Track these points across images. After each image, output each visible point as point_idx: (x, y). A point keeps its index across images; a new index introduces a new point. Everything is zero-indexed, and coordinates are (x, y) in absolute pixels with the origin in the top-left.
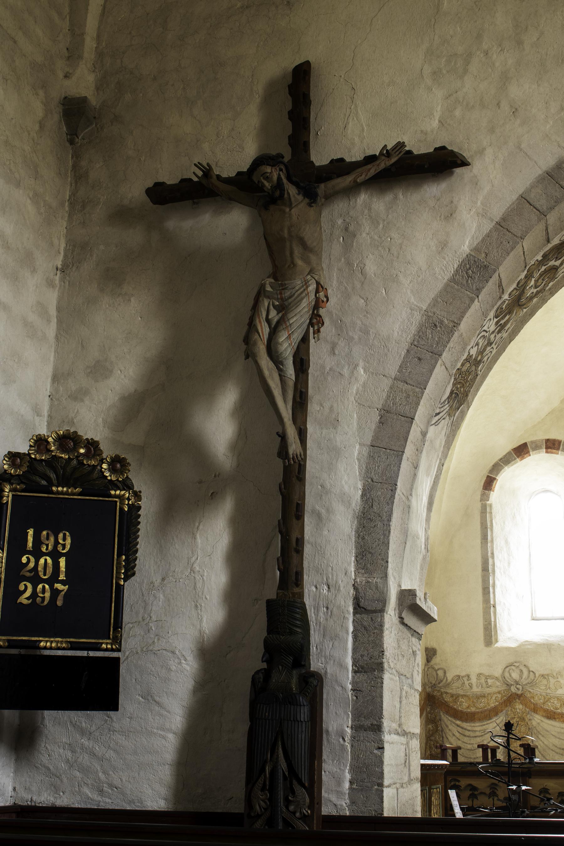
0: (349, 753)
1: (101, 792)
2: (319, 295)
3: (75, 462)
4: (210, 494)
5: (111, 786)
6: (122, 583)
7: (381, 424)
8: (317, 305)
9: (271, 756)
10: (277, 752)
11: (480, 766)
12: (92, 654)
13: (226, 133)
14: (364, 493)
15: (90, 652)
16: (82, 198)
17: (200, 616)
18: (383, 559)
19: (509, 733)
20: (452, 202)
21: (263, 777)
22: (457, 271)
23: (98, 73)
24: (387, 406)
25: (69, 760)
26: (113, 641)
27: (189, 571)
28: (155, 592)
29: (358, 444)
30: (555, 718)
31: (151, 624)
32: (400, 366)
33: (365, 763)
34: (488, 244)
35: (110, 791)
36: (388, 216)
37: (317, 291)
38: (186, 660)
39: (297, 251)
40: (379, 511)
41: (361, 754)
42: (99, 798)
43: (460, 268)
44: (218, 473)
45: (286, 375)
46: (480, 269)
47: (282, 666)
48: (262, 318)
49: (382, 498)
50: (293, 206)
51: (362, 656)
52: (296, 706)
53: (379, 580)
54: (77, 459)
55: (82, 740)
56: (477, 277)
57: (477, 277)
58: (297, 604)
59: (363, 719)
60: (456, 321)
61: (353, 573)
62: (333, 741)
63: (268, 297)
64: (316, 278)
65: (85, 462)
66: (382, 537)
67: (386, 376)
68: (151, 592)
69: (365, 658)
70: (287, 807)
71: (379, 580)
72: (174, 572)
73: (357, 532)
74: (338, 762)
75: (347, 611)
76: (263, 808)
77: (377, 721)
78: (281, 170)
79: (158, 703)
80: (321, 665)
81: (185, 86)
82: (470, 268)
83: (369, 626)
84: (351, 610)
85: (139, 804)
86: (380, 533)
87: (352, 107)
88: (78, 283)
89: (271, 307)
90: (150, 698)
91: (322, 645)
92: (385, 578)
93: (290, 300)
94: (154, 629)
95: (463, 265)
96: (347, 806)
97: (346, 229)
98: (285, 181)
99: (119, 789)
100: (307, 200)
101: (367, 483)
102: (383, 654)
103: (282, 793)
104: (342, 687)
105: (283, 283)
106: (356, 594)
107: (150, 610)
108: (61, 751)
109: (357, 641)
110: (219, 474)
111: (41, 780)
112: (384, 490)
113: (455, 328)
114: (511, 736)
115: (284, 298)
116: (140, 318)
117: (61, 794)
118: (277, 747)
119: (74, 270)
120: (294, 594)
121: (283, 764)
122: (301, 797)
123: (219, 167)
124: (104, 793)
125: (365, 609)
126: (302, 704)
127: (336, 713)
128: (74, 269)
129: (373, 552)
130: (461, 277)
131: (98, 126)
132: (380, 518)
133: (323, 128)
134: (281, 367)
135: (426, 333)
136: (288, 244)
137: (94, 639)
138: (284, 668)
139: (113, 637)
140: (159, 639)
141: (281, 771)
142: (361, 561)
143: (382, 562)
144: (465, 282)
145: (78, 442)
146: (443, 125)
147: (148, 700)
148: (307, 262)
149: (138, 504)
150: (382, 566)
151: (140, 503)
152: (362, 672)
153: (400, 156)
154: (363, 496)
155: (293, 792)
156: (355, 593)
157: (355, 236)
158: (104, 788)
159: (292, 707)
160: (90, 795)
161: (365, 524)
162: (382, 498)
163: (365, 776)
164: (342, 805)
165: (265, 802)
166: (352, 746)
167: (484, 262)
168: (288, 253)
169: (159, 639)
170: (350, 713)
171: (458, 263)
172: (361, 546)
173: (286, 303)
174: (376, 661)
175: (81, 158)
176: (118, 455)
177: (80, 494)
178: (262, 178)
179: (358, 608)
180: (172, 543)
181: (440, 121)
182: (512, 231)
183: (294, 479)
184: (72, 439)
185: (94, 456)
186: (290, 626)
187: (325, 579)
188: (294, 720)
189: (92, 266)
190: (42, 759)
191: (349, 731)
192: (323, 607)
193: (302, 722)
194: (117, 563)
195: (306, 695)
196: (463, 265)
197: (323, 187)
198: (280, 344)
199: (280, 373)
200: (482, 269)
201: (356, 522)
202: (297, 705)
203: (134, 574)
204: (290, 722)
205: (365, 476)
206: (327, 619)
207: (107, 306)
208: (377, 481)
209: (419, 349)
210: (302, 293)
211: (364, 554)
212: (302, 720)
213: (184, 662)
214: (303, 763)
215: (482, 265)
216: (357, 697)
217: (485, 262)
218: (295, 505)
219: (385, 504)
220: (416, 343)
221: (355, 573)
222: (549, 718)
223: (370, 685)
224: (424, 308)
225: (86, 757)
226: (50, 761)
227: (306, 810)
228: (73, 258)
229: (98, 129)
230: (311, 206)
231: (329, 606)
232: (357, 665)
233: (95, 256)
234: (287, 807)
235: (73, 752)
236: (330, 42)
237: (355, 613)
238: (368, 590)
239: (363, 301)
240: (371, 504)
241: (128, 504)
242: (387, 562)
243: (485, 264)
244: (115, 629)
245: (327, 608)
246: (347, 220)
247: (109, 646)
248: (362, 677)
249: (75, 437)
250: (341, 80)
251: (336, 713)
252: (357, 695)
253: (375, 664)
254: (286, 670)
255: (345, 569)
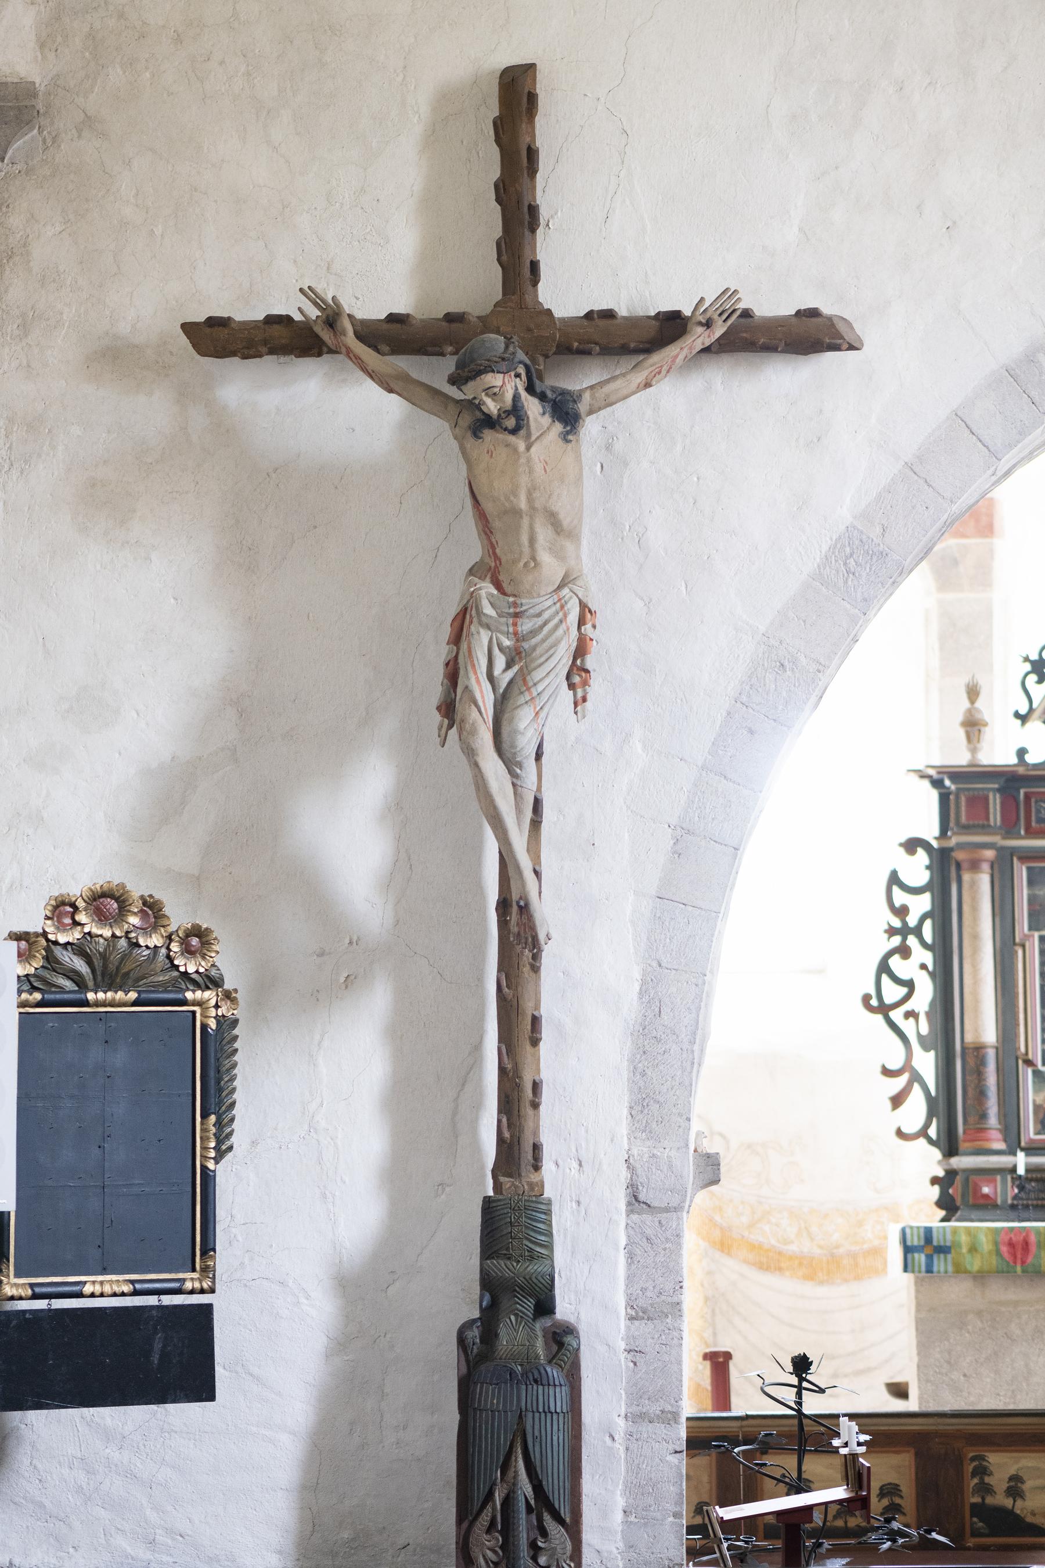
0: (623, 1460)
1: (152, 1543)
2: (585, 629)
3: (123, 942)
4: (342, 979)
5: (170, 1531)
6: (211, 1165)
7: (676, 856)
8: (581, 650)
9: (503, 1474)
10: (515, 1467)
11: (735, 1450)
12: (168, 1300)
13: (347, 195)
14: (644, 988)
15: (163, 1297)
16: (18, 307)
17: (332, 1215)
18: (680, 1115)
19: (801, 1379)
20: (821, 411)
21: (490, 1509)
22: (827, 559)
23: (42, 7)
24: (688, 820)
25: (82, 1488)
26: (200, 1275)
27: (306, 1127)
28: (239, 1167)
29: (632, 892)
30: (780, 1269)
31: (234, 1230)
32: (713, 743)
33: (651, 1479)
34: (889, 507)
35: (169, 1541)
36: (692, 427)
37: (581, 622)
38: (308, 1297)
39: (544, 534)
40: (672, 1024)
41: (643, 1462)
42: (148, 1556)
43: (833, 553)
44: (355, 939)
45: (524, 785)
46: (871, 559)
47: (516, 1315)
48: (481, 672)
49: (678, 999)
50: (533, 438)
51: (644, 1290)
52: (546, 1388)
53: (673, 1153)
54: (127, 937)
55: (108, 1451)
56: (864, 574)
57: (864, 574)
58: (540, 1206)
59: (646, 1401)
60: (822, 660)
61: (625, 1138)
62: (592, 1440)
63: (488, 627)
64: (580, 596)
65: (142, 942)
66: (679, 1073)
67: (685, 761)
68: (229, 1169)
69: (649, 1294)
70: (535, 1559)
71: (673, 1153)
72: (276, 1129)
73: (631, 1061)
74: (602, 1478)
75: (616, 1208)
76: (492, 1562)
77: (672, 1406)
78: (518, 376)
79: (257, 1379)
80: (568, 1305)
81: (250, 68)
82: (851, 555)
83: (656, 1236)
84: (622, 1206)
85: (229, 1563)
86: (675, 1066)
87: (622, 175)
88: (26, 509)
89: (496, 651)
90: (239, 1369)
91: (571, 1270)
92: (684, 1150)
93: (534, 641)
94: (240, 1239)
95: (839, 546)
96: (619, 1553)
97: (609, 447)
98: (523, 394)
99: (186, 1537)
100: (558, 427)
101: (649, 969)
102: (681, 1287)
103: (525, 1536)
104: (609, 1346)
105: (519, 602)
106: (631, 1178)
107: (231, 1201)
108: (66, 1471)
109: (633, 1262)
110: (359, 939)
111: (27, 1527)
112: (682, 984)
113: (820, 675)
114: (805, 1384)
115: (519, 632)
116: (172, 600)
117: (71, 1550)
118: (513, 1458)
119: (15, 478)
120: (532, 1186)
121: (526, 1487)
122: (557, 1542)
123: (336, 274)
124: (158, 1545)
125: (649, 1206)
126: (557, 1383)
127: (598, 1392)
128: (15, 474)
129: (662, 1100)
130: (834, 572)
131: (45, 132)
132: (675, 1037)
133: (559, 214)
134: (518, 771)
135: (764, 680)
136: (525, 522)
137: (170, 1272)
138: (519, 1319)
139: (201, 1268)
140: (252, 1259)
141: (523, 1497)
142: (641, 1116)
143: (679, 1119)
144: (841, 583)
145: (127, 904)
146: (808, 239)
147: (237, 1372)
148: (559, 555)
149: (233, 1014)
150: (680, 1126)
151: (235, 1012)
152: (643, 1318)
153: (730, 322)
154: (641, 993)
155: (544, 1533)
156: (629, 1176)
157: (626, 464)
158: (157, 1537)
159: (541, 1388)
160: (129, 1550)
161: (647, 1048)
162: (678, 999)
163: (650, 1500)
164: (611, 1552)
165: (495, 1552)
166: (627, 1449)
167: (879, 545)
168: (525, 539)
169: (252, 1259)
170: (623, 1392)
171: (829, 541)
172: (640, 1088)
173: (526, 645)
174: (670, 1300)
175: (8, 206)
176: (198, 924)
177: (136, 1003)
178: (483, 394)
179: (635, 1201)
180: (268, 1072)
181: (800, 229)
182: (934, 485)
183: (526, 969)
184: (117, 899)
185: (155, 927)
186: (530, 1245)
187: (574, 1150)
188: (544, 1411)
189: (56, 473)
190: (28, 1489)
191: (621, 1423)
192: (571, 1201)
193: (552, 1413)
194: (201, 1130)
195: (561, 1367)
196: (839, 546)
197: (588, 398)
198: (521, 733)
199: (515, 780)
200: (875, 559)
201: (629, 1044)
202: (549, 1385)
203: (230, 1148)
204: (537, 1415)
205: (647, 956)
206: (578, 1224)
207: (98, 567)
208: (669, 967)
209: (751, 711)
210: (556, 627)
211: (645, 1104)
212: (558, 1410)
213: (305, 1301)
214: (561, 1484)
215: (874, 550)
216: (635, 1364)
217: (882, 545)
218: (529, 1019)
219: (683, 1010)
220: (744, 699)
221: (629, 1139)
222: (764, 1267)
223: (659, 1342)
224: (762, 629)
225: (116, 1481)
226: (43, 1491)
227: (568, 1562)
228: (10, 448)
229: (44, 141)
230: (568, 441)
231: (582, 1200)
232: (635, 1307)
233: (60, 448)
234: (535, 1559)
235: (90, 1472)
236: (575, 12)
237: (630, 1212)
238: (654, 1170)
239: (641, 604)
240: (657, 1010)
241: (216, 1017)
242: (689, 1119)
243: (881, 549)
244: (204, 1253)
245: (579, 1203)
246: (610, 428)
247: (197, 1285)
248: (642, 1327)
249: (122, 895)
250: (600, 108)
251: (598, 1392)
252: (634, 1360)
253: (668, 1304)
254: (523, 1323)
255: (610, 1132)
